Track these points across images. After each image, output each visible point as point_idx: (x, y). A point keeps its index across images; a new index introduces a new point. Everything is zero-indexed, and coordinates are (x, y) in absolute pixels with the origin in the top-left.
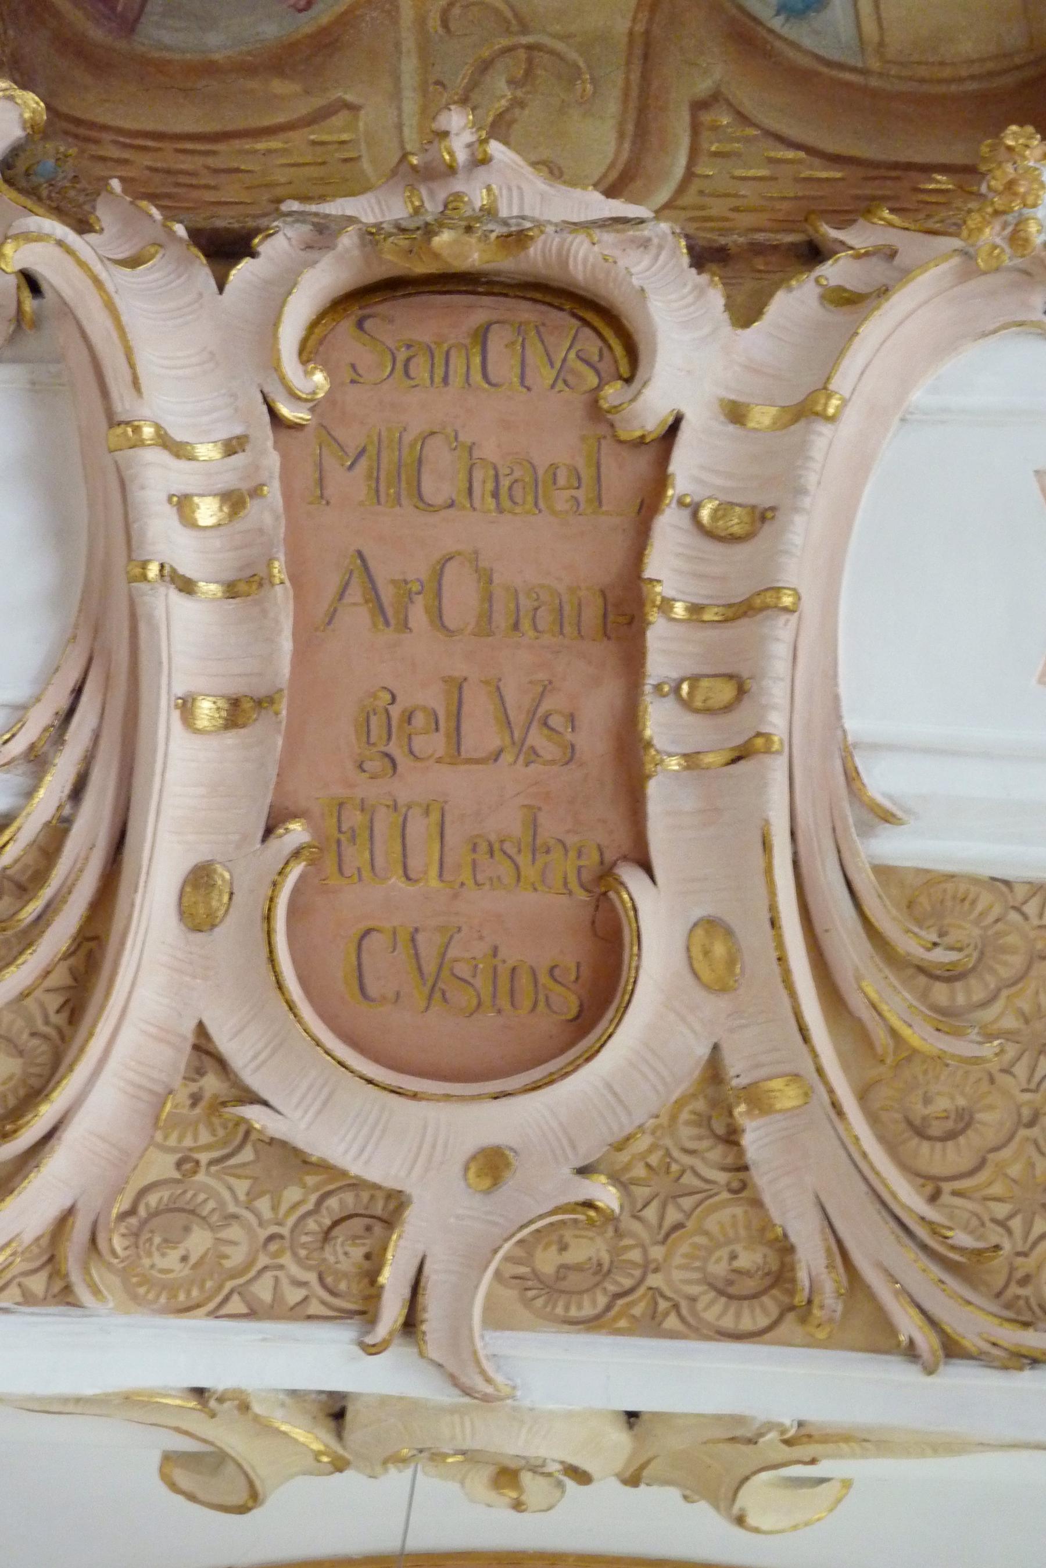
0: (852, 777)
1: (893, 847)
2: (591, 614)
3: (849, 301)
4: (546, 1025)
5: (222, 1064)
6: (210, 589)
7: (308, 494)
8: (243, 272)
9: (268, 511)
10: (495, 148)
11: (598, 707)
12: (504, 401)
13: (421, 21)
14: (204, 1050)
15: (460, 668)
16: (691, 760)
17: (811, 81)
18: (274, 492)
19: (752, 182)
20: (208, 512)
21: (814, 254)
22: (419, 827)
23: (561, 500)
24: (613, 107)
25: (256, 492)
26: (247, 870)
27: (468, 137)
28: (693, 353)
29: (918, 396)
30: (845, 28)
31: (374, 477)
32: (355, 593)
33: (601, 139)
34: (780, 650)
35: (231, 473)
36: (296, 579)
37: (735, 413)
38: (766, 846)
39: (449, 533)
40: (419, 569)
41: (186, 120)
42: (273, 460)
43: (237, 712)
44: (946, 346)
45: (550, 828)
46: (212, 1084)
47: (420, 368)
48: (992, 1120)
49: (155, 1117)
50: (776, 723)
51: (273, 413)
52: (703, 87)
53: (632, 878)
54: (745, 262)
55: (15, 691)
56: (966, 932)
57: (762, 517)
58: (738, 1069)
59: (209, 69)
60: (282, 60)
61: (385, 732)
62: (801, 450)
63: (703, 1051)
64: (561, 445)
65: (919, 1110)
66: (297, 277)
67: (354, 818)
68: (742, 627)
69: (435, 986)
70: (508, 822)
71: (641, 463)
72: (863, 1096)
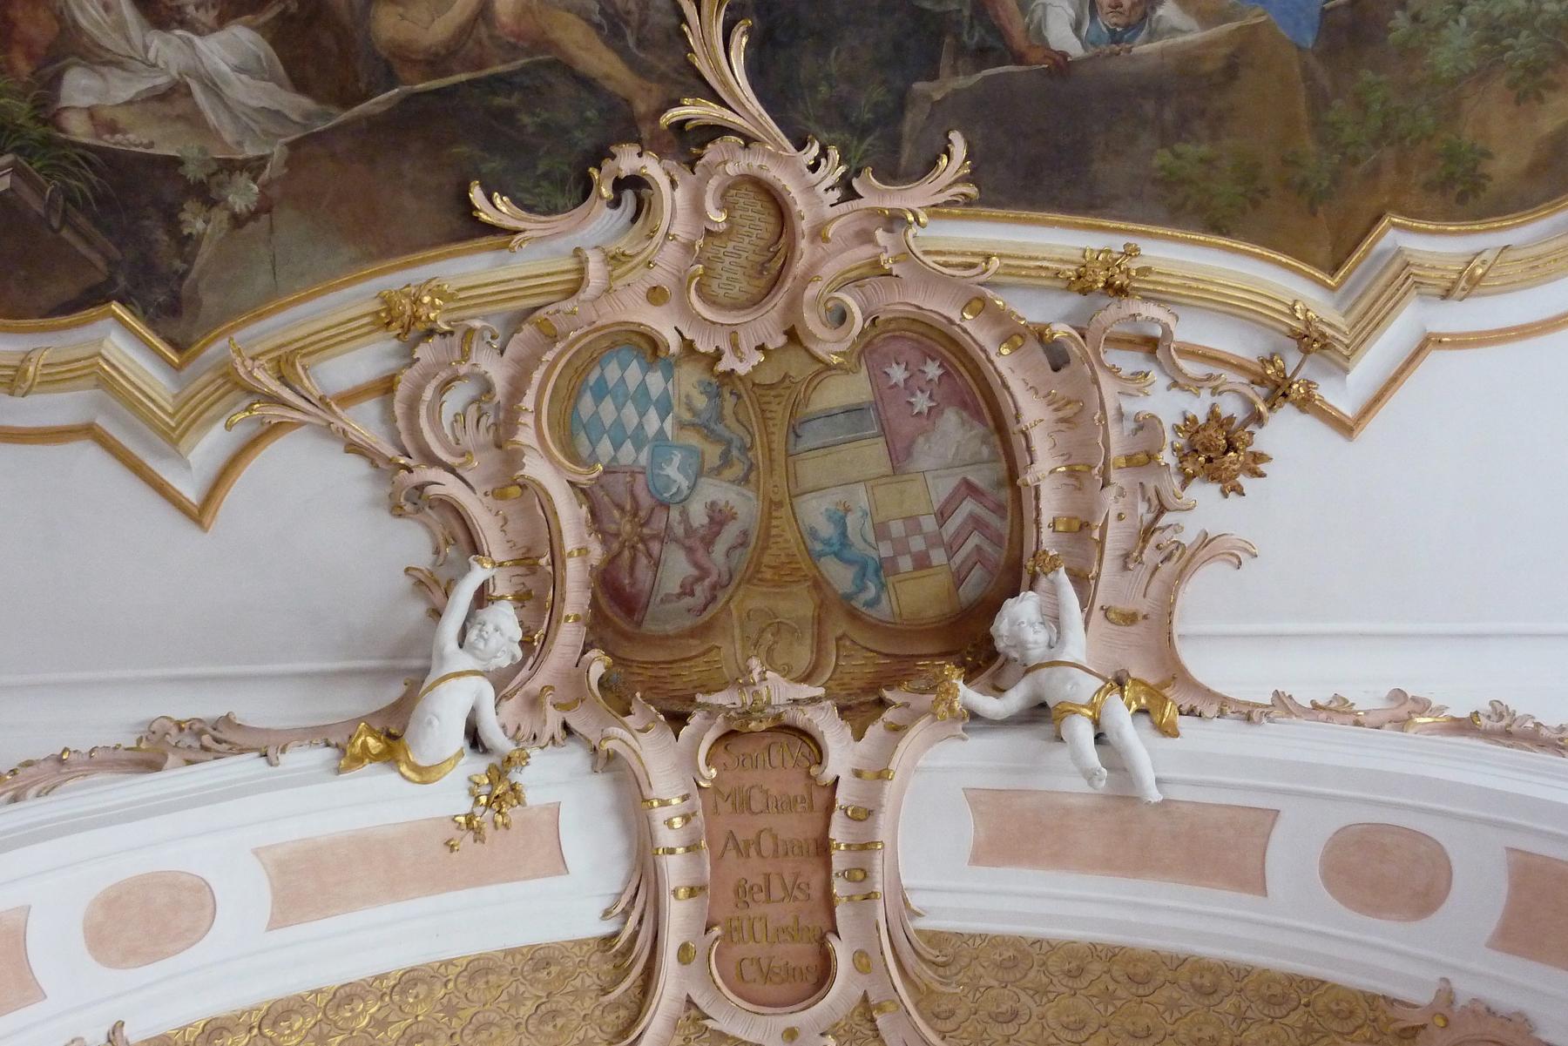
0: (906, 901)
1: (921, 924)
2: (812, 848)
3: (897, 730)
4: (807, 986)
5: (696, 1006)
6: (680, 850)
7: (712, 812)
8: (685, 731)
9: (699, 821)
10: (769, 674)
11: (816, 881)
12: (777, 775)
13: (740, 617)
14: (690, 1002)
15: (769, 870)
16: (850, 898)
17: (876, 627)
18: (700, 813)
19: (860, 666)
20: (678, 823)
21: (882, 704)
22: (758, 926)
23: (799, 807)
24: (809, 641)
25: (694, 814)
26: (700, 943)
27: (758, 669)
28: (842, 753)
29: (921, 762)
30: (888, 610)
31: (734, 804)
32: (730, 845)
33: (803, 656)
34: (878, 862)
35: (684, 808)
36: (709, 843)
37: (858, 774)
38: (878, 929)
39: (762, 822)
40: (751, 836)
41: (661, 655)
42: (699, 802)
43: (692, 892)
44: (929, 745)
45: (803, 923)
46: (693, 1012)
47: (748, 763)
48: (961, 1013)
49: (675, 1026)
50: (878, 888)
51: (699, 786)
52: (839, 632)
53: (831, 938)
54: (860, 709)
55: (618, 889)
56: (950, 950)
57: (870, 813)
58: (873, 999)
59: (667, 637)
60: (693, 633)
61: (743, 893)
62: (881, 790)
63: (861, 993)
64: (798, 788)
65: (937, 1010)
66: (702, 731)
67: (735, 923)
68: (864, 854)
69: (767, 976)
70: (788, 921)
71: (826, 794)
72: (916, 1005)
